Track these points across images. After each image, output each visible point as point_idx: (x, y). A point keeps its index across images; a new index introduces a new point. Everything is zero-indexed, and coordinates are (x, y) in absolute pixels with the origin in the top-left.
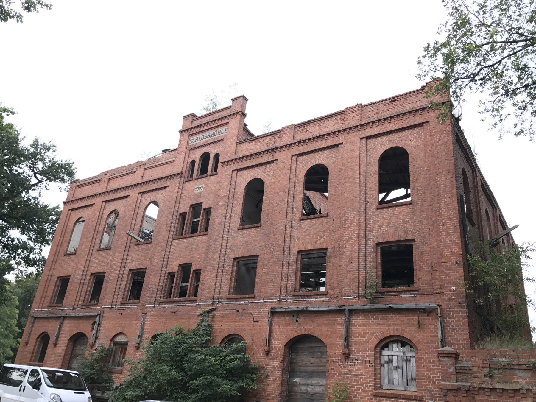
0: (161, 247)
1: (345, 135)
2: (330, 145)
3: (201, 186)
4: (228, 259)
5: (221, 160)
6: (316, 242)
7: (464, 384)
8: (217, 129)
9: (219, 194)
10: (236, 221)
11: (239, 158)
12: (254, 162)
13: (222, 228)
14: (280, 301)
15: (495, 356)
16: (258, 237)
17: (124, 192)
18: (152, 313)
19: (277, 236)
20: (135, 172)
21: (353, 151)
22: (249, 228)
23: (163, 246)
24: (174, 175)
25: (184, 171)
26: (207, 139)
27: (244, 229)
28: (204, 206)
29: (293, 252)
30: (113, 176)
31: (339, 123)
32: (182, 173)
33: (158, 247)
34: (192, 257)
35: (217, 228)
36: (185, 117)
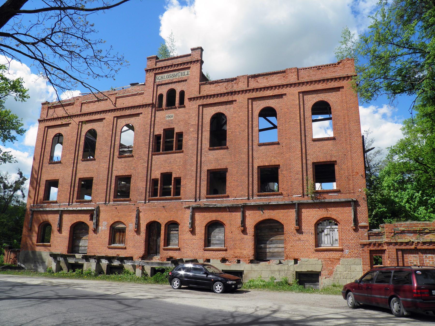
0: (143, 159)
1: (288, 88)
2: (276, 94)
7: (372, 240)
9: (189, 122)
10: (206, 143)
12: (216, 100)
14: (248, 199)
15: (397, 227)
18: (144, 207)
19: (242, 156)
21: (294, 100)
26: (171, 78)
28: (176, 131)
33: (140, 159)
34: (172, 168)
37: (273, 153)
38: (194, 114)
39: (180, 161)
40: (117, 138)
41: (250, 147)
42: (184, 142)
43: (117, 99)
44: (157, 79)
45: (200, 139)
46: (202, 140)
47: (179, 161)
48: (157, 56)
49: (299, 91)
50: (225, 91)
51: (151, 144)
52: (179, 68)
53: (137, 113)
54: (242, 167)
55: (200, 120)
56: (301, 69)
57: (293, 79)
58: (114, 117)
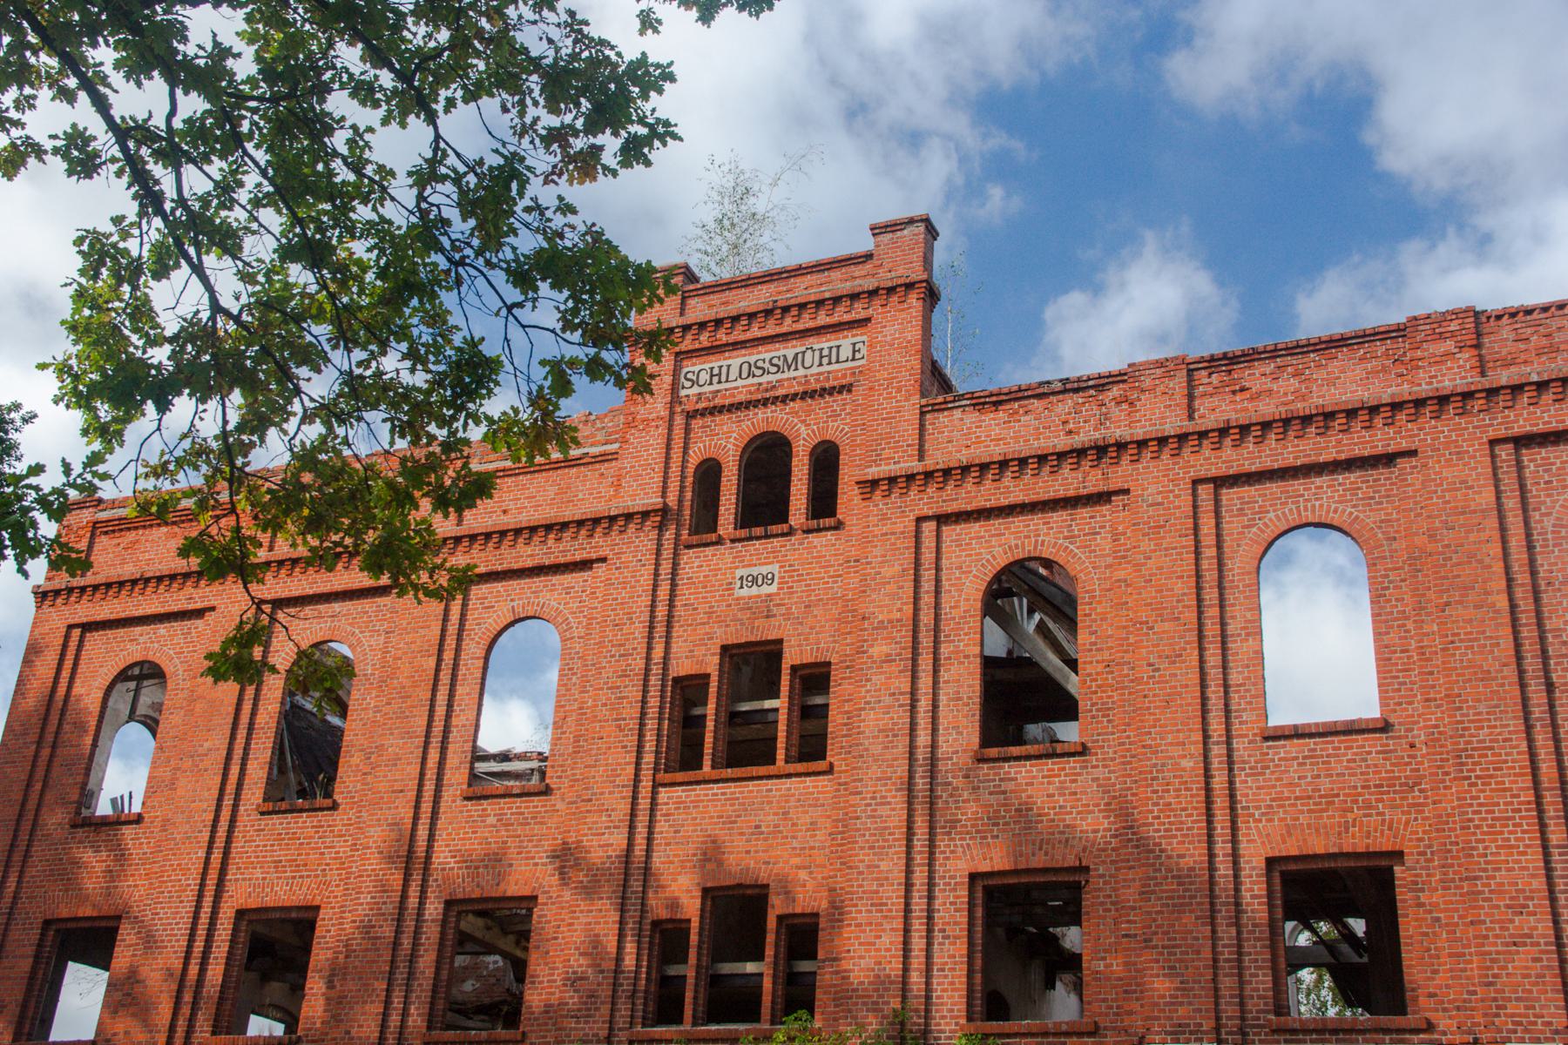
3: (764, 570)
12: (1013, 490)
24: (629, 517)
28: (792, 656)
32: (664, 511)
38: (893, 567)
39: (813, 827)
40: (460, 690)
41: (1217, 751)
42: (835, 718)
45: (924, 704)
46: (935, 707)
48: (687, 267)
49: (1492, 434)
50: (1062, 443)
51: (651, 724)
52: (806, 322)
53: (578, 558)
55: (927, 599)
56: (1499, 317)
57: (1456, 375)
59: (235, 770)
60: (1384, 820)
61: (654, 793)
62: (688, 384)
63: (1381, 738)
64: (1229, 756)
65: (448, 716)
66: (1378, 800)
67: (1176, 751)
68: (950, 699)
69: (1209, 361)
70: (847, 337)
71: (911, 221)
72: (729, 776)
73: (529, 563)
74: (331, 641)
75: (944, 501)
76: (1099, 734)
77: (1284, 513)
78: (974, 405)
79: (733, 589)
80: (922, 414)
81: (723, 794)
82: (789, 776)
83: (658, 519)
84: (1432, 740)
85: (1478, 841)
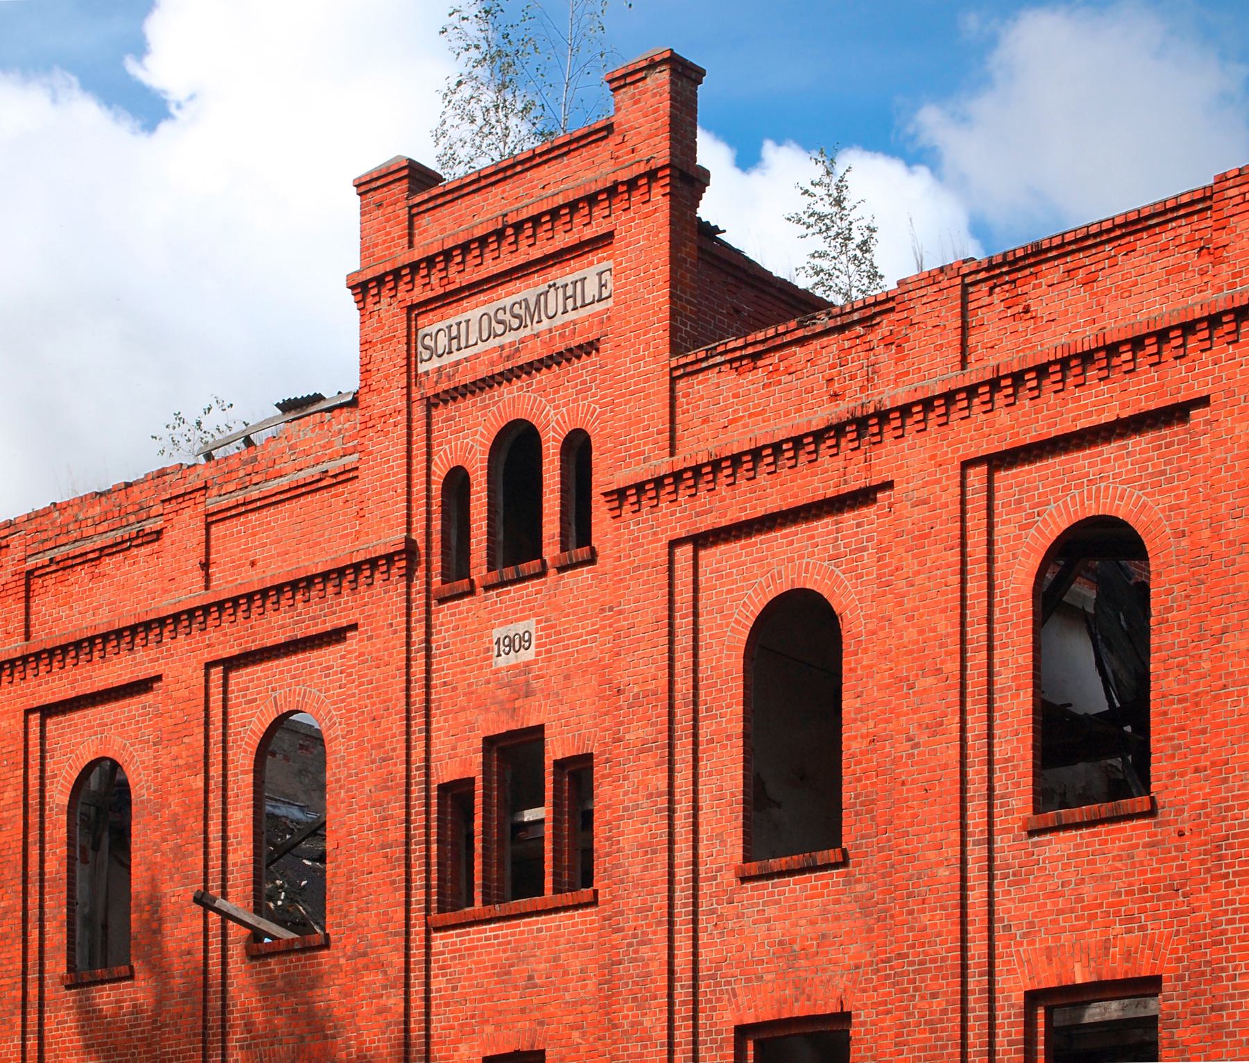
0: (381, 965)
3: (520, 627)
4: (709, 1033)
5: (606, 475)
6: (1106, 946)
8: (555, 271)
11: (697, 470)
13: (661, 870)
16: (837, 918)
17: (126, 658)
19: (925, 919)
20: (159, 534)
22: (790, 873)
23: (390, 964)
24: (373, 563)
25: (418, 535)
27: (770, 876)
28: (556, 749)
29: (1007, 998)
30: (45, 558)
31: (1184, 268)
32: (410, 550)
35: (636, 870)
36: (365, 187)
37: (1121, 886)
41: (976, 853)
43: (213, 529)
44: (426, 355)
47: (576, 966)
51: (418, 850)
53: (329, 627)
54: (924, 1005)
55: (683, 660)
58: (209, 666)
59: (34, 934)
60: (1145, 936)
61: (428, 940)
62: (426, 355)
63: (1148, 826)
64: (991, 859)
65: (225, 853)
66: (1143, 910)
67: (932, 856)
68: (713, 799)
69: (987, 270)
70: (591, 264)
71: (652, 65)
72: (499, 914)
73: (282, 638)
74: (297, 712)
75: (698, 515)
76: (862, 837)
77: (1065, 503)
78: (731, 361)
79: (491, 657)
80: (673, 381)
81: (496, 937)
82: (557, 910)
83: (403, 564)
84: (1198, 826)
85: (1229, 960)
